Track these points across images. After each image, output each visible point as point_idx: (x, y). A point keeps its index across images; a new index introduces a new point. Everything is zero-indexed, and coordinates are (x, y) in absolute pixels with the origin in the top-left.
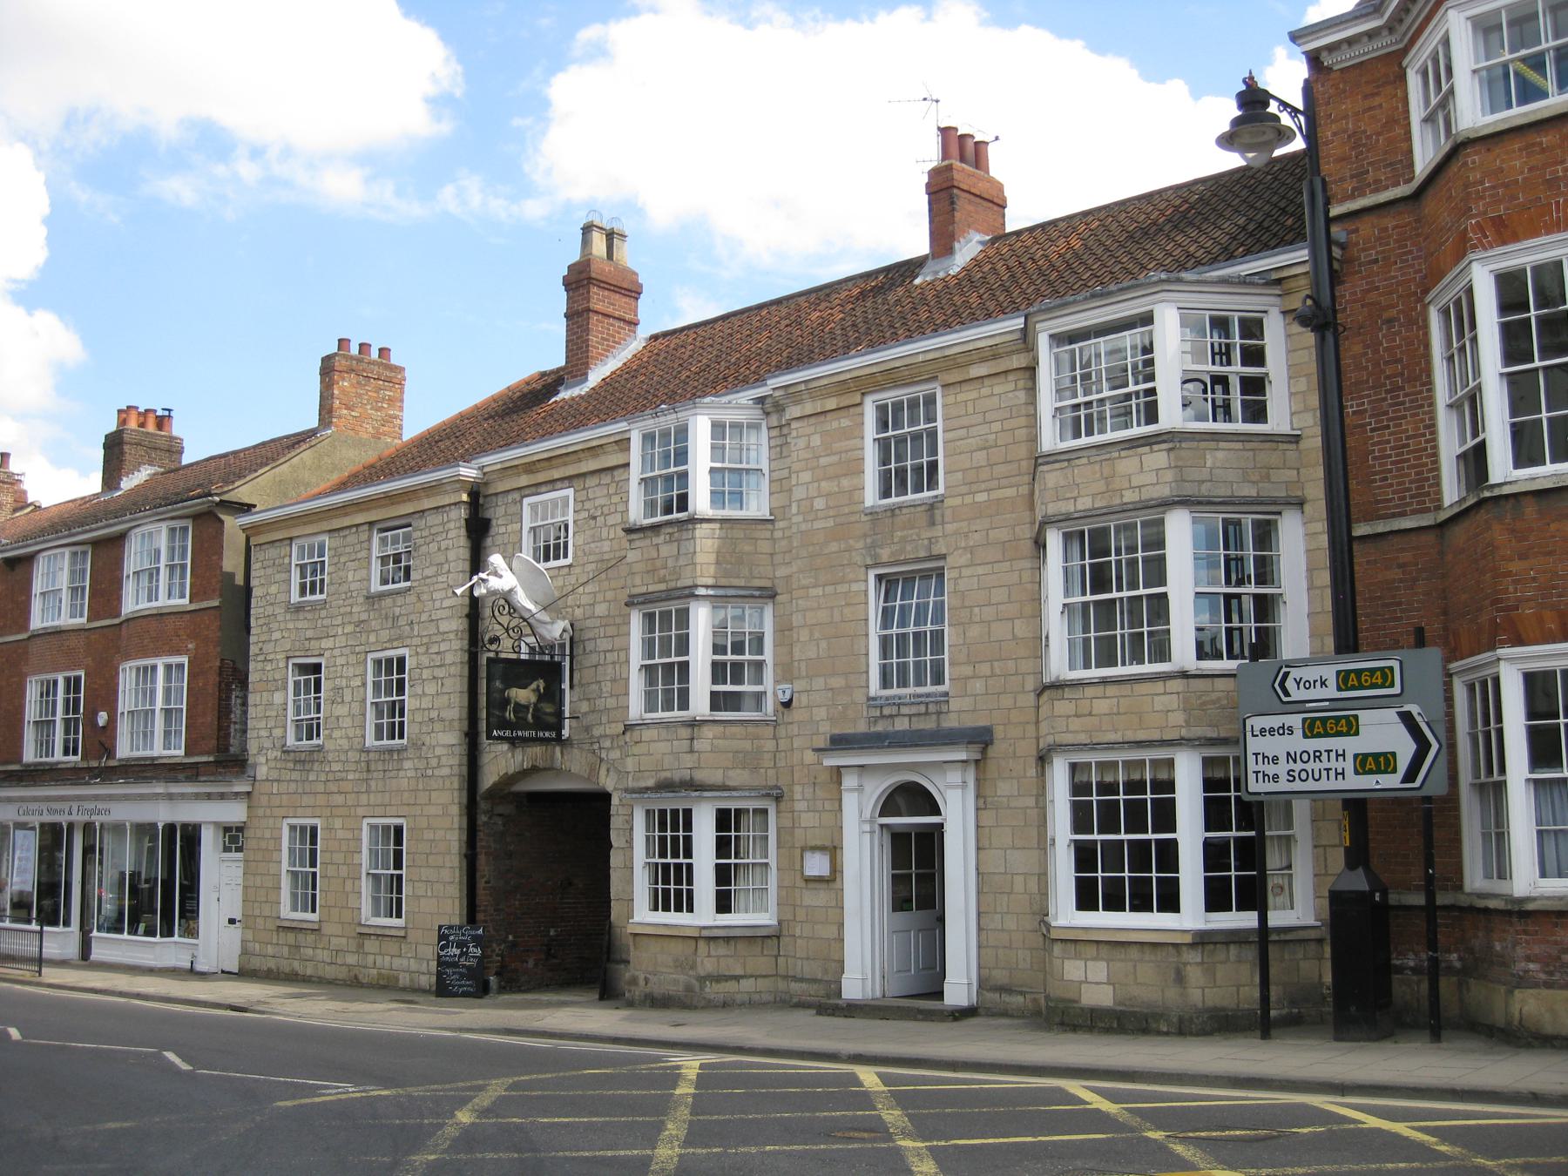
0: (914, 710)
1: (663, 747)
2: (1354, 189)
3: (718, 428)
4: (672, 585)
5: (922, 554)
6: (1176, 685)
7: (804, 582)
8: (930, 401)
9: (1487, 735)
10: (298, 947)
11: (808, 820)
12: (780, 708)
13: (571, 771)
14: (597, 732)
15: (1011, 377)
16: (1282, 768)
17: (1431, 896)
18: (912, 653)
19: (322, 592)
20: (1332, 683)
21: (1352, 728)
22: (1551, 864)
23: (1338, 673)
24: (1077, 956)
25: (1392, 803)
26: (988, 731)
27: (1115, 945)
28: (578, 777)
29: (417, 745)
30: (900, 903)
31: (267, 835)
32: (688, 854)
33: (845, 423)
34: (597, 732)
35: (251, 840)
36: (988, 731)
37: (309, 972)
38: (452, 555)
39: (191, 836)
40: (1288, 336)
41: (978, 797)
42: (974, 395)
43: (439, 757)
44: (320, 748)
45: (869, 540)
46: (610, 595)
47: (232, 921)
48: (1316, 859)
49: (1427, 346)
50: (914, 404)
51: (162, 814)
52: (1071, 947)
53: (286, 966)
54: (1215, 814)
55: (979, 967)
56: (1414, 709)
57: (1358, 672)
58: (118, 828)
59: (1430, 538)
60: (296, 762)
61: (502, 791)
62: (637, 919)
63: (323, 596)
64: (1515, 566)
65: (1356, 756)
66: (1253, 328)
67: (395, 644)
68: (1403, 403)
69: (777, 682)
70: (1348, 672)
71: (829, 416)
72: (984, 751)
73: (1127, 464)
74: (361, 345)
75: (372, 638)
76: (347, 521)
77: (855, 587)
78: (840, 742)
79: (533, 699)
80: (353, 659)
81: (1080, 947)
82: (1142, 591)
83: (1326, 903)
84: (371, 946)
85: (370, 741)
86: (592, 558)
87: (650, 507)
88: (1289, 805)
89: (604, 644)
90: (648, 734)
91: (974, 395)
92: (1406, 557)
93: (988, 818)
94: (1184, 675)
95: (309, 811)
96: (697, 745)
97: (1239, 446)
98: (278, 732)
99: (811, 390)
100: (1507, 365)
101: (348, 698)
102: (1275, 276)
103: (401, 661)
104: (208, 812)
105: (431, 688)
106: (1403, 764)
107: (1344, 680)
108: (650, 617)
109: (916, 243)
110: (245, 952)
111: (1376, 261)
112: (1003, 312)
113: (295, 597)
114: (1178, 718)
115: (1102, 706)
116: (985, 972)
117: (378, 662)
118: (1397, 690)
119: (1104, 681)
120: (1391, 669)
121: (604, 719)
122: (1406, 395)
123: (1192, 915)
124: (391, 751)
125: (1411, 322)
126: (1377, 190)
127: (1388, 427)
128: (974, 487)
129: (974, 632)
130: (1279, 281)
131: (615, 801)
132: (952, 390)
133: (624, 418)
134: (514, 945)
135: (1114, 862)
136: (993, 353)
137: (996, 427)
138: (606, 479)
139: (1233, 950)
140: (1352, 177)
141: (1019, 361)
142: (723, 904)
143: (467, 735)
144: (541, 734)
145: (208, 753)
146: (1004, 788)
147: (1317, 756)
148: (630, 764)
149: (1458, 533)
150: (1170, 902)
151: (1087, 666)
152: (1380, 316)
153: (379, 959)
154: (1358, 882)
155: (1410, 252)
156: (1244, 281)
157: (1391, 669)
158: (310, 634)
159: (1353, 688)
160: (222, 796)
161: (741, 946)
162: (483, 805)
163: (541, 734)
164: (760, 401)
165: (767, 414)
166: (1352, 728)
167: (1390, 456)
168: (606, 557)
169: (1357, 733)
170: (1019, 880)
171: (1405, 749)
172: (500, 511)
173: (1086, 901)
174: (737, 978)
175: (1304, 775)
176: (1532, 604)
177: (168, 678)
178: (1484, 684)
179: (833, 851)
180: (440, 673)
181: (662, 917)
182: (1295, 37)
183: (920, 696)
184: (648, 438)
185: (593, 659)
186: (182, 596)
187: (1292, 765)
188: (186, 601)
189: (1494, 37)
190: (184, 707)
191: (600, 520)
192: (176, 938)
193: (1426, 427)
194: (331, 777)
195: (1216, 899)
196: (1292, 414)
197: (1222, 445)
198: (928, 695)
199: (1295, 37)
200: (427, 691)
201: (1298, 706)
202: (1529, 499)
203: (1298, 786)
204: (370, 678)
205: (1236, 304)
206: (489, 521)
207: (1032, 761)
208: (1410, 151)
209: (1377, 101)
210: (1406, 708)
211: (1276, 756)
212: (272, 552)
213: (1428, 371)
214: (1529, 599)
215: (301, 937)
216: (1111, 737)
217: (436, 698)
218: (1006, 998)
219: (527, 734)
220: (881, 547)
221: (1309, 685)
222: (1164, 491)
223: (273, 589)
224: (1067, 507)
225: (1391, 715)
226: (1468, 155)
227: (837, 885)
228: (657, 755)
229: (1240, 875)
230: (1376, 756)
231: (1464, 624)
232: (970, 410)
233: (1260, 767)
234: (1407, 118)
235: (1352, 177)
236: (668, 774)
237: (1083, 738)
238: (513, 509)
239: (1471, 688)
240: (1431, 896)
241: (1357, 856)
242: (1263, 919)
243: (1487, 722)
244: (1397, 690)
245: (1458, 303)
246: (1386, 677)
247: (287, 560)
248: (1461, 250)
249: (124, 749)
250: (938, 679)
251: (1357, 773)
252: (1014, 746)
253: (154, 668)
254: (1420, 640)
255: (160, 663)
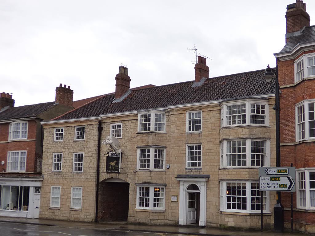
0: (195, 171)
1: (144, 175)
2: (283, 83)
3: (156, 115)
4: (147, 145)
5: (197, 142)
6: (248, 170)
7: (173, 146)
8: (200, 113)
9: (302, 182)
10: (54, 213)
11: (172, 190)
12: (167, 169)
13: (121, 178)
14: (127, 171)
15: (216, 111)
16: (266, 186)
17: (292, 209)
18: (195, 161)
19: (62, 139)
20: (276, 172)
21: (279, 179)
22: (313, 204)
23: (277, 170)
24: (227, 217)
25: (285, 193)
26: (209, 175)
27: (235, 215)
28: (122, 180)
29: (85, 172)
30: (190, 207)
31: (47, 189)
32: (148, 196)
33: (182, 116)
34: (127, 171)
35: (42, 190)
36: (209, 175)
37: (57, 218)
38: (94, 134)
39: (27, 189)
40: (269, 109)
41: (207, 187)
42: (209, 114)
43: (91, 175)
44: (61, 172)
45: (187, 139)
46: (130, 145)
47: (37, 207)
48: (270, 201)
49: (295, 113)
50: (196, 114)
51: (19, 184)
52: (226, 215)
53: (51, 217)
54: (253, 193)
55: (206, 219)
56: (290, 177)
57: (281, 170)
58: (7, 187)
59: (293, 147)
60: (55, 174)
61: (103, 182)
62: (137, 208)
63: (62, 140)
64: (309, 154)
65: (280, 184)
66: (263, 107)
67: (81, 151)
68: (290, 123)
69: (166, 164)
70: (279, 170)
71: (179, 115)
72: (208, 179)
73: (240, 130)
74: (64, 85)
75: (75, 150)
76: (69, 125)
77: (183, 147)
78: (179, 176)
79: (114, 164)
80: (70, 154)
81: (228, 215)
82: (241, 153)
83: (273, 209)
84: (72, 212)
85: (73, 171)
86: (126, 137)
87: (142, 129)
88: (266, 192)
89: (128, 154)
90: (141, 173)
91: (209, 114)
92: (289, 150)
93: (209, 191)
94: (249, 168)
95: (58, 185)
96: (151, 175)
97: (260, 128)
98: (50, 168)
99: (176, 110)
100: (310, 119)
101: (68, 162)
102: (268, 98)
103: (82, 155)
104: (32, 184)
105: (89, 161)
106: (288, 186)
107: (278, 171)
108: (141, 151)
109: (192, 78)
110: (40, 214)
111: (286, 97)
112: (217, 99)
113: (55, 140)
114: (247, 176)
115: (233, 173)
116: (207, 220)
117: (76, 155)
118: (287, 173)
119: (234, 168)
120: (286, 170)
121: (128, 169)
122: (290, 122)
123: (248, 210)
124: (79, 173)
125: (292, 109)
126: (287, 84)
127: (287, 127)
128: (208, 131)
129: (207, 157)
130: (268, 99)
131: (130, 185)
132: (204, 112)
133: (135, 109)
134: (104, 213)
135: (234, 201)
136: (213, 106)
137: (213, 120)
138: (130, 122)
139: (256, 217)
140: (283, 81)
141: (218, 108)
142: (155, 206)
143: (97, 171)
144: (116, 171)
145: (32, 172)
146: (212, 186)
147: (273, 184)
148: (137, 178)
149: (299, 147)
150: (245, 207)
151: (230, 165)
152: (286, 107)
153: (75, 216)
154: (279, 206)
155: (293, 96)
156: (262, 99)
157: (286, 170)
158: (59, 148)
159: (280, 173)
160: (36, 181)
161: (158, 213)
162: (100, 185)
163: (116, 171)
164: (165, 110)
165: (166, 113)
166: (279, 179)
167: (287, 132)
168: (130, 137)
169: (280, 180)
170: (214, 204)
171: (288, 183)
172: (105, 126)
173: (229, 207)
174: (157, 220)
175: (270, 187)
176: (311, 160)
177: (22, 155)
178: (302, 173)
179: (178, 196)
180: (91, 158)
181: (142, 208)
182: (275, 54)
183: (196, 168)
184: (142, 116)
185: (126, 157)
186: (25, 138)
187: (268, 185)
188: (26, 139)
189: (311, 61)
190: (26, 161)
191: (128, 130)
192: (22, 211)
193: (294, 127)
194: (64, 178)
195: (253, 207)
196: (269, 123)
197: (257, 128)
198: (198, 168)
199: (275, 54)
200: (88, 161)
201: (269, 175)
202: (312, 143)
203: (269, 189)
204: (74, 158)
205: (260, 103)
206: (102, 128)
207: (218, 181)
208: (294, 78)
209: (289, 68)
210: (289, 177)
211: (265, 184)
212: (49, 130)
213: (294, 118)
214: (311, 160)
215: (55, 211)
216: (234, 178)
217: (89, 163)
218: (211, 224)
219: (113, 171)
220: (189, 140)
221: (272, 172)
222: (247, 136)
223: (49, 138)
224: (228, 137)
225: (286, 178)
226: (305, 82)
227: (178, 203)
228: (144, 176)
229: (258, 204)
230: (283, 185)
231: (299, 162)
232: (208, 116)
233: (262, 185)
234: (294, 72)
235: (283, 81)
236: (145, 181)
237: (230, 178)
238: (109, 126)
239: (299, 173)
240: (292, 209)
241: (278, 201)
242: (262, 211)
243: (302, 180)
244: (287, 173)
245: (301, 107)
246: (285, 171)
247: (53, 132)
248: (303, 98)
249: (9, 170)
250: (199, 165)
251: (280, 187)
252: (214, 179)
253: (18, 153)
254: (292, 166)
255: (20, 152)
